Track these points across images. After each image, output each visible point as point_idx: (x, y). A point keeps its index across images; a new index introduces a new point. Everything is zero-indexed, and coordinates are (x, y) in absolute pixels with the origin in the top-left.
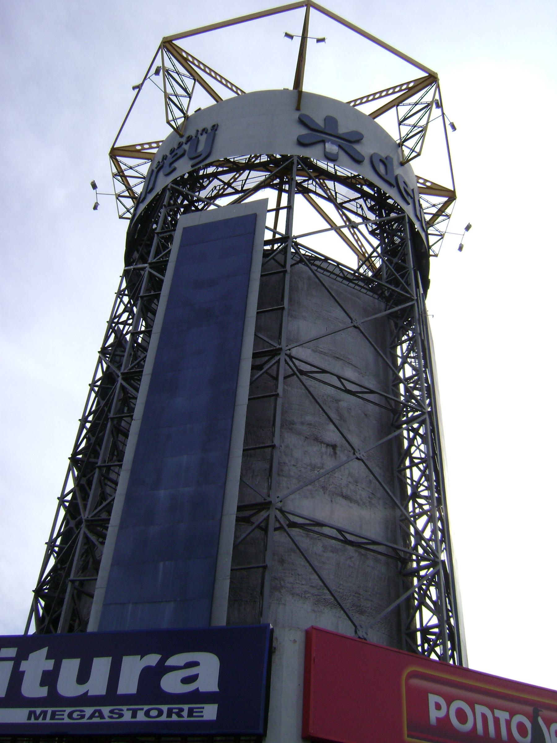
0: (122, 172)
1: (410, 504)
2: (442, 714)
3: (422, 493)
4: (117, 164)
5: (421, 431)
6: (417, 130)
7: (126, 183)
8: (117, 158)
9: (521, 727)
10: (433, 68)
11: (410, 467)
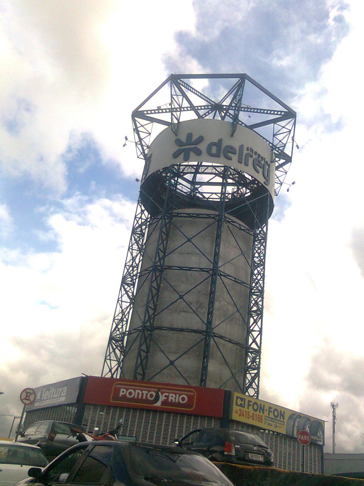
2: (123, 394)
3: (259, 246)
4: (134, 121)
9: (151, 396)
10: (240, 70)
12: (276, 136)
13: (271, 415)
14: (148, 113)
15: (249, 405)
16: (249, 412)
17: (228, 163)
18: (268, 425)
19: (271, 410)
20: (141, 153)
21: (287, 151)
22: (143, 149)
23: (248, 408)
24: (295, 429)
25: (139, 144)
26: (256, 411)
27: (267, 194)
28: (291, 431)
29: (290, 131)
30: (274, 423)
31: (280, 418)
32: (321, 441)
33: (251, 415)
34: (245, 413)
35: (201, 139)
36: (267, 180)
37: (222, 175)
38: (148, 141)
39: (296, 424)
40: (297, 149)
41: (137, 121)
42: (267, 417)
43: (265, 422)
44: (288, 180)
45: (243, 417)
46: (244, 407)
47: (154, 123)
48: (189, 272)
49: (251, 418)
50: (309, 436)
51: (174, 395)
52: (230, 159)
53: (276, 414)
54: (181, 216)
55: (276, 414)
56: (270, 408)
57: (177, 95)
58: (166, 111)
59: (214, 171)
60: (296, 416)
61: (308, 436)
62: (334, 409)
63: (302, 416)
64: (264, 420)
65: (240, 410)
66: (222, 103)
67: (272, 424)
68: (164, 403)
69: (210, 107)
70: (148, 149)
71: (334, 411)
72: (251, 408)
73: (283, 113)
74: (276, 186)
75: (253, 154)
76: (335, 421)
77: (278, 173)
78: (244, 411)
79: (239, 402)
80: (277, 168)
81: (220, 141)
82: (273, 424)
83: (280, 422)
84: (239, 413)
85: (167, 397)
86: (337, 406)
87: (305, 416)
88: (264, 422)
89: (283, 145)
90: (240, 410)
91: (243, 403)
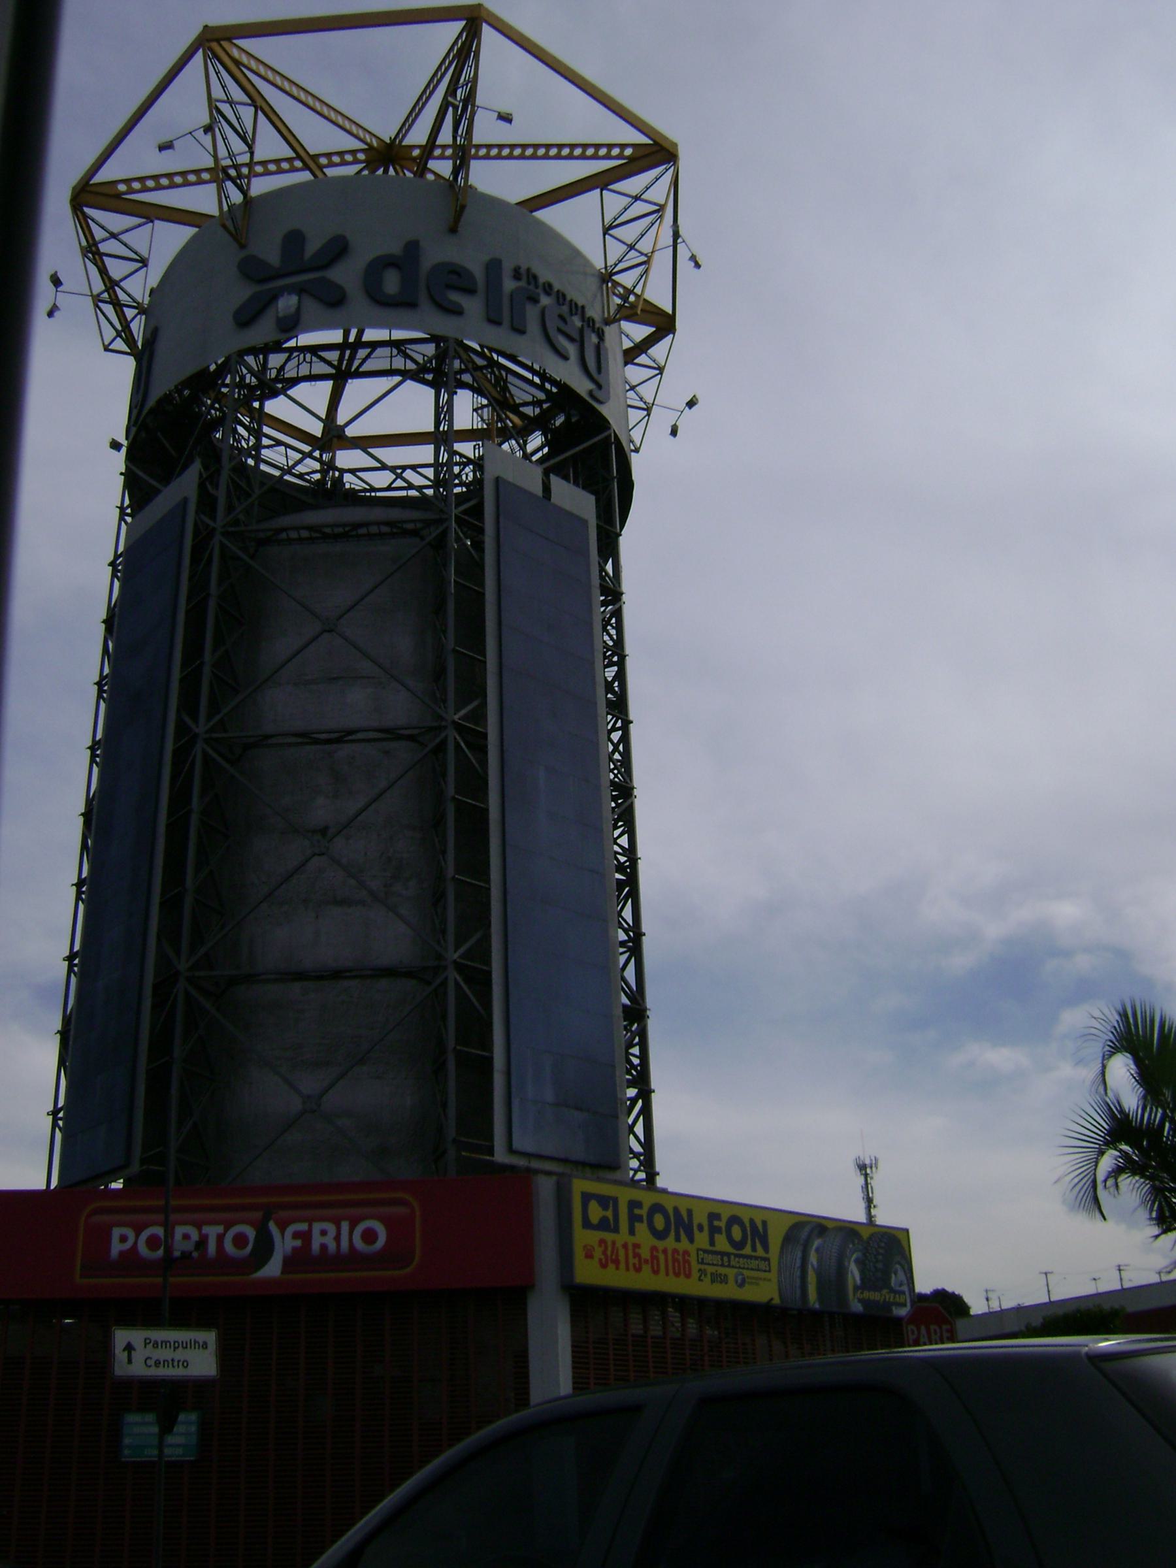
0: (96, 244)
1: (331, 172)
4: (83, 222)
5: (611, 748)
6: (640, 208)
7: (100, 264)
8: (86, 209)
9: (240, 1240)
10: (670, 128)
11: (258, 459)
12: (611, 232)
13: (722, 1243)
14: (132, 191)
15: (634, 1219)
16: (636, 1246)
17: (446, 326)
18: (713, 1282)
19: (716, 1223)
20: (119, 335)
21: (657, 294)
22: (121, 316)
23: (632, 1232)
24: (812, 1278)
25: (106, 302)
26: (661, 1235)
27: (606, 434)
28: (798, 1292)
29: (661, 208)
30: (735, 1271)
31: (754, 1249)
32: (904, 1305)
33: (645, 1253)
34: (622, 1253)
35: (338, 249)
36: (599, 387)
37: (429, 377)
38: (138, 287)
39: (813, 1259)
40: (696, 270)
41: (93, 220)
42: (705, 1251)
43: (702, 1272)
44: (671, 392)
45: (617, 1268)
46: (616, 1230)
47: (157, 222)
48: (344, 751)
49: (646, 1269)
50: (948, 1327)
51: (331, 1228)
52: (457, 311)
53: (737, 1233)
54: (290, 541)
55: (737, 1233)
56: (713, 1217)
57: (231, 102)
58: (199, 177)
59: (399, 363)
60: (807, 1229)
61: (945, 1327)
62: (866, 1175)
63: (830, 1225)
64: (695, 1266)
65: (602, 1242)
66: (401, 141)
67: (726, 1275)
68: (296, 1261)
69: (361, 156)
70: (144, 317)
71: (867, 1183)
72: (642, 1228)
73: (628, 152)
74: (634, 416)
75: (540, 291)
76: (873, 1212)
77: (634, 373)
78: (619, 1244)
79: (596, 1212)
80: (630, 356)
81: (412, 249)
82: (731, 1273)
83: (754, 1264)
84: (598, 1253)
85: (306, 1236)
86: (874, 1164)
87: (839, 1224)
88: (695, 1274)
89: (644, 259)
90: (602, 1242)
91: (609, 1214)
